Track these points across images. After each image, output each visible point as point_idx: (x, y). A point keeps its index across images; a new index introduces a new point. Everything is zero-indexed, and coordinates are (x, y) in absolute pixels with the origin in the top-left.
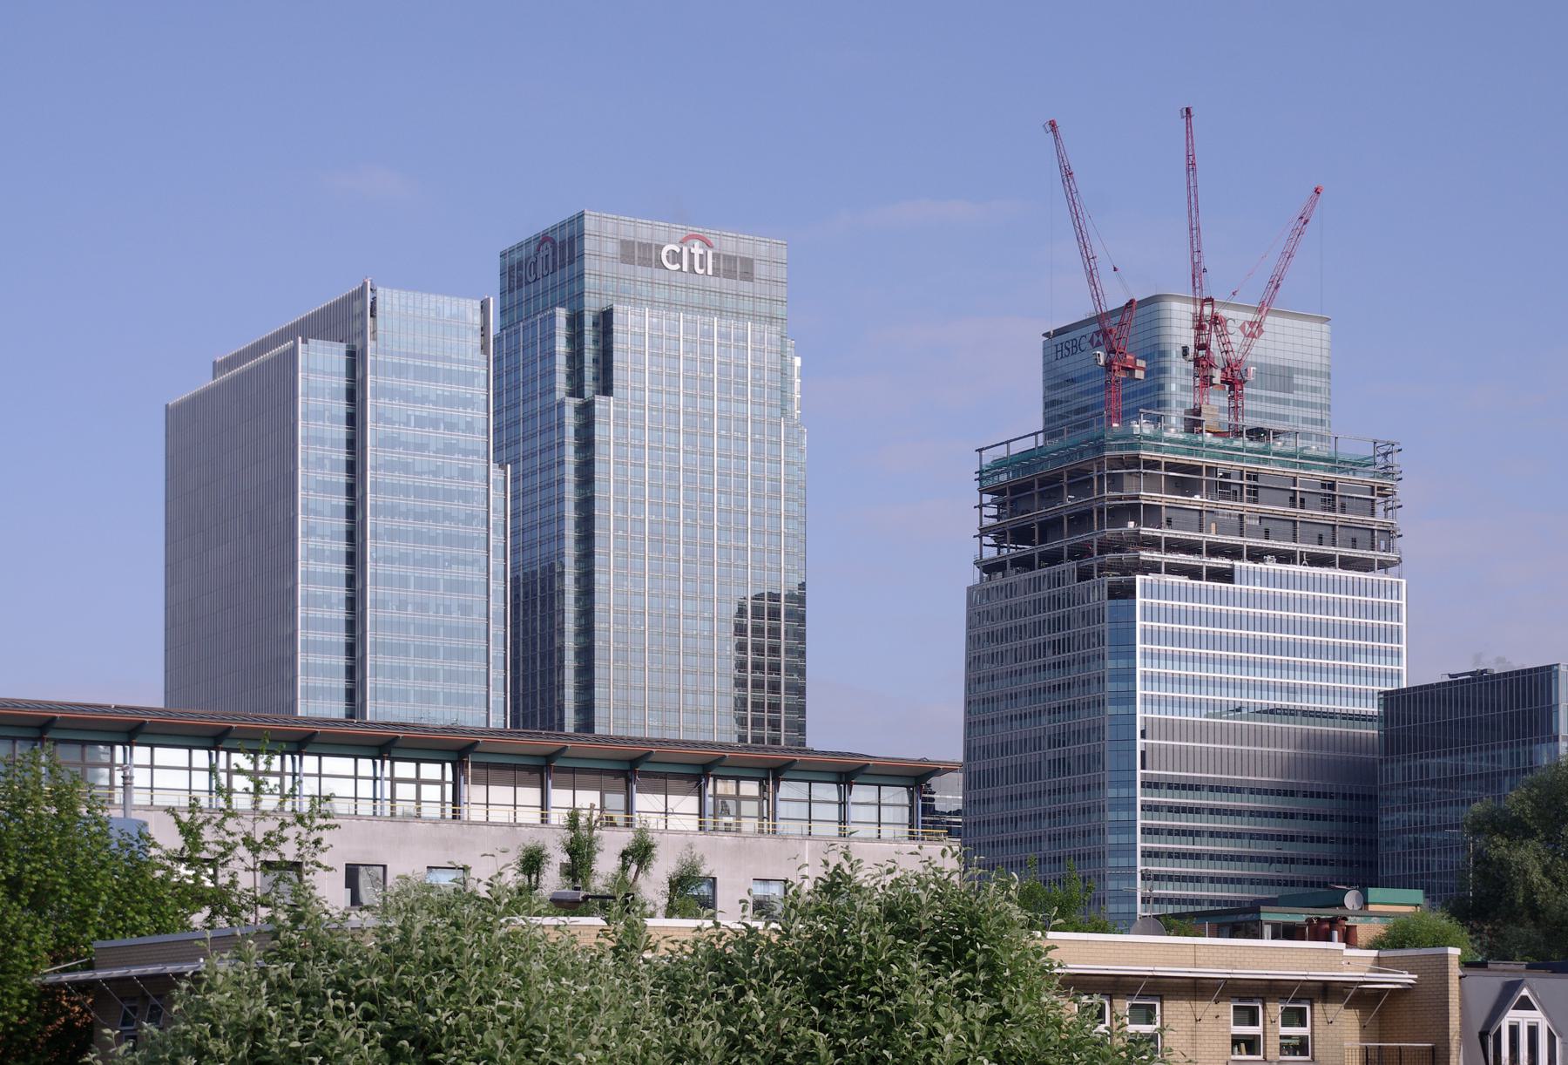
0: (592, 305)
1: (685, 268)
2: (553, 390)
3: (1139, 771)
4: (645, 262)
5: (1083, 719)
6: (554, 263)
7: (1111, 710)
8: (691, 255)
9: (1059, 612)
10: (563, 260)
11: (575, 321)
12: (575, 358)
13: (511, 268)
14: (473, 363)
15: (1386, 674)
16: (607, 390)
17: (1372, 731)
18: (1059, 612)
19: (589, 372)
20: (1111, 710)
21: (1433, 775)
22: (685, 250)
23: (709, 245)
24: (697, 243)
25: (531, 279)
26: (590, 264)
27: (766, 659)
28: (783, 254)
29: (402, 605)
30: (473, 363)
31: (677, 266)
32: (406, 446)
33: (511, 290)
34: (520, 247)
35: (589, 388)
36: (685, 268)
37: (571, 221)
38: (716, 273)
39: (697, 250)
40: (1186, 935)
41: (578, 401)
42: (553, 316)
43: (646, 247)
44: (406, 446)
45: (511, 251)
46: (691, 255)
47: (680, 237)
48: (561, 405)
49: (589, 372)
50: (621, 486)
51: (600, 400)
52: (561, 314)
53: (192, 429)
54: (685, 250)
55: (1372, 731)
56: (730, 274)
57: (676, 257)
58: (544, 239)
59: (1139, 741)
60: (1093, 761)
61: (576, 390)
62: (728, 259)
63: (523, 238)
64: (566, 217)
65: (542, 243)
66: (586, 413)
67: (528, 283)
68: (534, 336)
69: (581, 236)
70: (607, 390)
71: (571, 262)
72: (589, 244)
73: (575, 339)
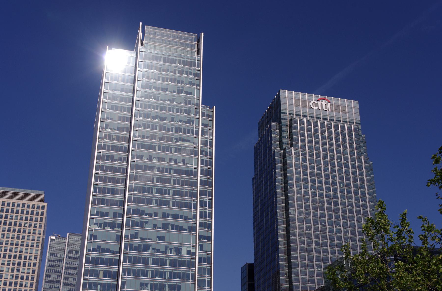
24: (324, 101)
29: (150, 158)
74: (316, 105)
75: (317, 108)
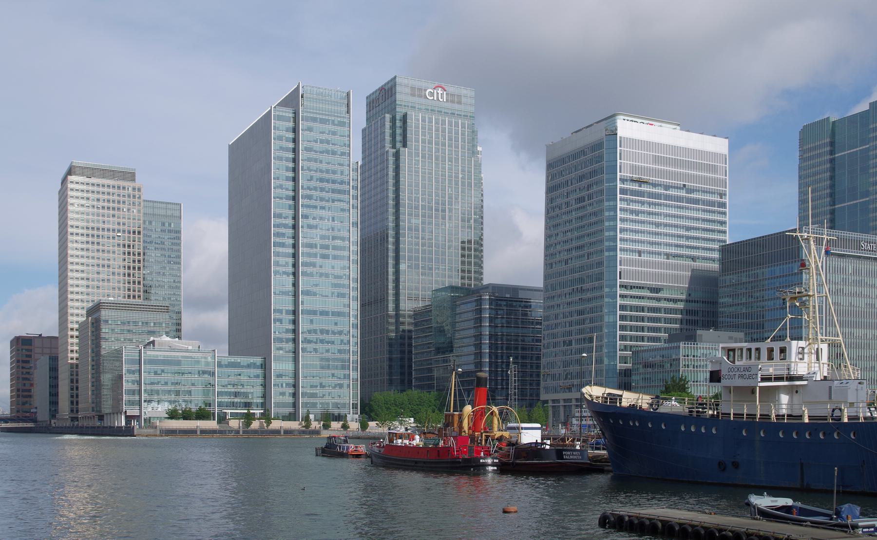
3: (619, 280)
5: (595, 258)
7: (606, 254)
9: (312, 400)
11: (393, 120)
12: (393, 135)
15: (719, 241)
16: (405, 146)
17: (716, 266)
18: (312, 400)
19: (399, 138)
20: (606, 254)
21: (728, 283)
28: (473, 94)
35: (398, 145)
37: (391, 80)
38: (447, 101)
39: (440, 91)
41: (394, 150)
44: (316, 152)
48: (387, 152)
49: (399, 138)
52: (388, 116)
55: (716, 266)
57: (432, 94)
58: (382, 89)
59: (619, 267)
60: (600, 277)
61: (394, 147)
63: (374, 90)
64: (390, 79)
66: (397, 155)
70: (405, 146)
72: (398, 89)
73: (393, 127)
74: (432, 94)
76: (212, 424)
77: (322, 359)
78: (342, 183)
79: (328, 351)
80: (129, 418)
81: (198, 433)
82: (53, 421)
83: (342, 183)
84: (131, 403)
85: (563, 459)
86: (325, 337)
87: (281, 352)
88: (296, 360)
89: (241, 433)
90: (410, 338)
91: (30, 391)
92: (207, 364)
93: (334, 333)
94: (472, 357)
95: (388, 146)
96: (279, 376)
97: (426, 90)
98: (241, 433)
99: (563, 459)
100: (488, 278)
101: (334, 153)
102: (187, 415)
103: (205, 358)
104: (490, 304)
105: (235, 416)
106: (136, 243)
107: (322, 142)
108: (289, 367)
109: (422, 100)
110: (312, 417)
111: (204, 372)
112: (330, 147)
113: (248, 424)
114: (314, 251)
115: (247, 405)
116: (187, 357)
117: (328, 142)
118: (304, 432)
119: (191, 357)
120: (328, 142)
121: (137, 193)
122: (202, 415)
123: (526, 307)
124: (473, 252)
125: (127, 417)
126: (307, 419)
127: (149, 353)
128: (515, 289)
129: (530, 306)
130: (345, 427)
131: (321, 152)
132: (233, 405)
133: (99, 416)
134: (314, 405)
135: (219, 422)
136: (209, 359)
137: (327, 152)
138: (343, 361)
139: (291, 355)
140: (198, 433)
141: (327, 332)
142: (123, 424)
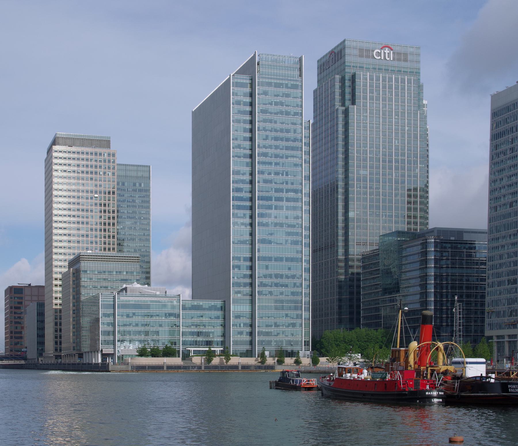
0: (349, 71)
1: (382, 58)
2: (334, 105)
4: (368, 57)
6: (335, 60)
8: (385, 53)
10: (338, 58)
13: (321, 66)
14: (296, 81)
16: (353, 103)
19: (348, 97)
22: (382, 51)
23: (392, 50)
24: (387, 49)
25: (327, 68)
26: (347, 58)
27: (412, 193)
30: (296, 81)
31: (380, 57)
32: (287, 86)
33: (321, 73)
34: (324, 57)
35: (347, 103)
36: (382, 58)
37: (341, 44)
38: (394, 59)
40: (471, 357)
41: (344, 108)
42: (334, 78)
43: (368, 51)
44: (271, 113)
45: (321, 59)
46: (385, 53)
47: (381, 47)
48: (337, 110)
49: (348, 97)
50: (359, 140)
51: (351, 107)
52: (338, 77)
53: (199, 116)
54: (382, 51)
56: (399, 60)
57: (379, 54)
58: (332, 52)
61: (343, 105)
62: (399, 54)
64: (339, 42)
65: (331, 54)
66: (346, 113)
67: (326, 69)
68: (328, 87)
69: (344, 48)
70: (353, 103)
71: (341, 58)
72: (347, 51)
75: (380, 57)
76: (177, 361)
77: (276, 301)
78: (295, 140)
79: (282, 294)
80: (105, 356)
81: (165, 368)
82: (40, 359)
83: (295, 140)
84: (107, 343)
85: (508, 392)
86: (279, 280)
87: (239, 295)
88: (252, 302)
89: (203, 368)
90: (359, 280)
91: (21, 333)
92: (173, 307)
93: (287, 277)
94: (418, 297)
95: (338, 104)
96: (237, 317)
97: (373, 51)
98: (203, 368)
99: (508, 392)
100: (432, 224)
101: (288, 113)
102: (155, 353)
103: (172, 302)
104: (435, 247)
105: (197, 353)
106: (111, 202)
107: (276, 104)
108: (246, 308)
109: (370, 60)
110: (267, 353)
111: (170, 315)
112: (284, 108)
113: (209, 360)
114: (269, 203)
115: (209, 343)
116: (156, 302)
117: (282, 104)
118: (260, 367)
119: (159, 302)
120: (282, 104)
121: (111, 158)
122: (168, 352)
123: (471, 248)
124: (418, 197)
125: (103, 355)
126: (262, 355)
127: (122, 298)
128: (460, 233)
129: (475, 248)
130: (298, 362)
131: (275, 114)
132: (196, 343)
133: (79, 354)
134: (269, 343)
135: (183, 359)
136: (175, 303)
137: (281, 113)
138: (296, 302)
139: (248, 298)
140: (165, 368)
141: (281, 276)
142: (100, 361)
